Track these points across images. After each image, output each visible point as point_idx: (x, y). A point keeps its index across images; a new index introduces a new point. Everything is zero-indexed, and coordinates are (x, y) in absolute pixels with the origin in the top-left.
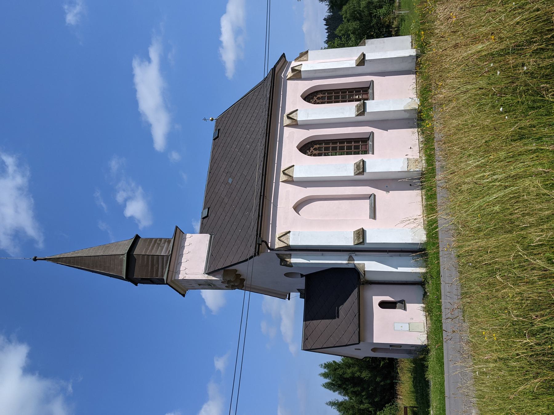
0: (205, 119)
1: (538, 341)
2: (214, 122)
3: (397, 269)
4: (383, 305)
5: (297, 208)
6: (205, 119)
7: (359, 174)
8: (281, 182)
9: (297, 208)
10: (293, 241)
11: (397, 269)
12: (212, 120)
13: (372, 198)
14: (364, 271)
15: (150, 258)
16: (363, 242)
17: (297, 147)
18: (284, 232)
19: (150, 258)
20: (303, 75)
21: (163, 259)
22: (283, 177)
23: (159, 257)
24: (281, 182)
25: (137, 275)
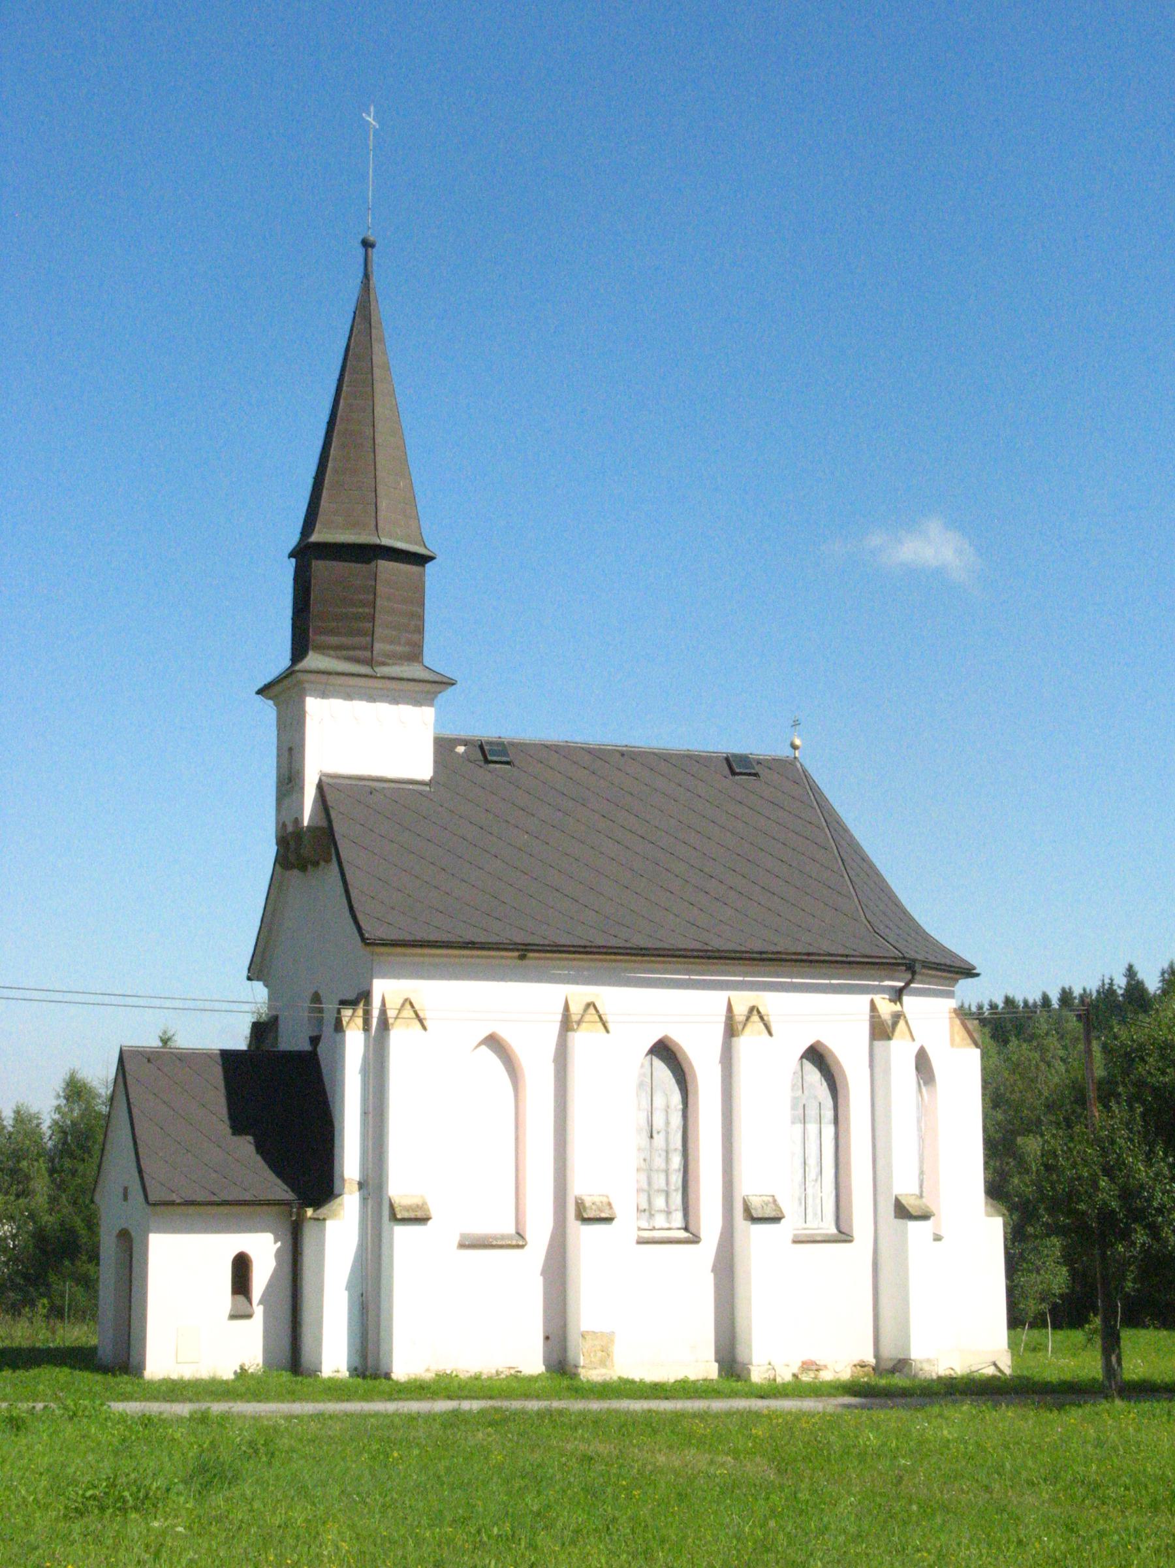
0: (796, 723)
1: (768, 1516)
2: (784, 752)
3: (258, 1305)
4: (241, 1267)
5: (665, 1051)
6: (796, 723)
7: (747, 1210)
8: (872, 1002)
9: (665, 1051)
10: (401, 1038)
11: (258, 1305)
12: (794, 747)
13: (517, 1241)
14: (324, 1219)
15: (367, 610)
16: (394, 1218)
17: (818, 1042)
18: (952, 1026)
19: (367, 610)
20: (878, 1044)
21: (364, 648)
22: (742, 1000)
23: (365, 635)
24: (872, 1002)
25: (320, 568)
